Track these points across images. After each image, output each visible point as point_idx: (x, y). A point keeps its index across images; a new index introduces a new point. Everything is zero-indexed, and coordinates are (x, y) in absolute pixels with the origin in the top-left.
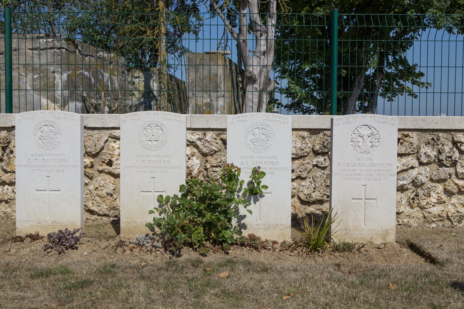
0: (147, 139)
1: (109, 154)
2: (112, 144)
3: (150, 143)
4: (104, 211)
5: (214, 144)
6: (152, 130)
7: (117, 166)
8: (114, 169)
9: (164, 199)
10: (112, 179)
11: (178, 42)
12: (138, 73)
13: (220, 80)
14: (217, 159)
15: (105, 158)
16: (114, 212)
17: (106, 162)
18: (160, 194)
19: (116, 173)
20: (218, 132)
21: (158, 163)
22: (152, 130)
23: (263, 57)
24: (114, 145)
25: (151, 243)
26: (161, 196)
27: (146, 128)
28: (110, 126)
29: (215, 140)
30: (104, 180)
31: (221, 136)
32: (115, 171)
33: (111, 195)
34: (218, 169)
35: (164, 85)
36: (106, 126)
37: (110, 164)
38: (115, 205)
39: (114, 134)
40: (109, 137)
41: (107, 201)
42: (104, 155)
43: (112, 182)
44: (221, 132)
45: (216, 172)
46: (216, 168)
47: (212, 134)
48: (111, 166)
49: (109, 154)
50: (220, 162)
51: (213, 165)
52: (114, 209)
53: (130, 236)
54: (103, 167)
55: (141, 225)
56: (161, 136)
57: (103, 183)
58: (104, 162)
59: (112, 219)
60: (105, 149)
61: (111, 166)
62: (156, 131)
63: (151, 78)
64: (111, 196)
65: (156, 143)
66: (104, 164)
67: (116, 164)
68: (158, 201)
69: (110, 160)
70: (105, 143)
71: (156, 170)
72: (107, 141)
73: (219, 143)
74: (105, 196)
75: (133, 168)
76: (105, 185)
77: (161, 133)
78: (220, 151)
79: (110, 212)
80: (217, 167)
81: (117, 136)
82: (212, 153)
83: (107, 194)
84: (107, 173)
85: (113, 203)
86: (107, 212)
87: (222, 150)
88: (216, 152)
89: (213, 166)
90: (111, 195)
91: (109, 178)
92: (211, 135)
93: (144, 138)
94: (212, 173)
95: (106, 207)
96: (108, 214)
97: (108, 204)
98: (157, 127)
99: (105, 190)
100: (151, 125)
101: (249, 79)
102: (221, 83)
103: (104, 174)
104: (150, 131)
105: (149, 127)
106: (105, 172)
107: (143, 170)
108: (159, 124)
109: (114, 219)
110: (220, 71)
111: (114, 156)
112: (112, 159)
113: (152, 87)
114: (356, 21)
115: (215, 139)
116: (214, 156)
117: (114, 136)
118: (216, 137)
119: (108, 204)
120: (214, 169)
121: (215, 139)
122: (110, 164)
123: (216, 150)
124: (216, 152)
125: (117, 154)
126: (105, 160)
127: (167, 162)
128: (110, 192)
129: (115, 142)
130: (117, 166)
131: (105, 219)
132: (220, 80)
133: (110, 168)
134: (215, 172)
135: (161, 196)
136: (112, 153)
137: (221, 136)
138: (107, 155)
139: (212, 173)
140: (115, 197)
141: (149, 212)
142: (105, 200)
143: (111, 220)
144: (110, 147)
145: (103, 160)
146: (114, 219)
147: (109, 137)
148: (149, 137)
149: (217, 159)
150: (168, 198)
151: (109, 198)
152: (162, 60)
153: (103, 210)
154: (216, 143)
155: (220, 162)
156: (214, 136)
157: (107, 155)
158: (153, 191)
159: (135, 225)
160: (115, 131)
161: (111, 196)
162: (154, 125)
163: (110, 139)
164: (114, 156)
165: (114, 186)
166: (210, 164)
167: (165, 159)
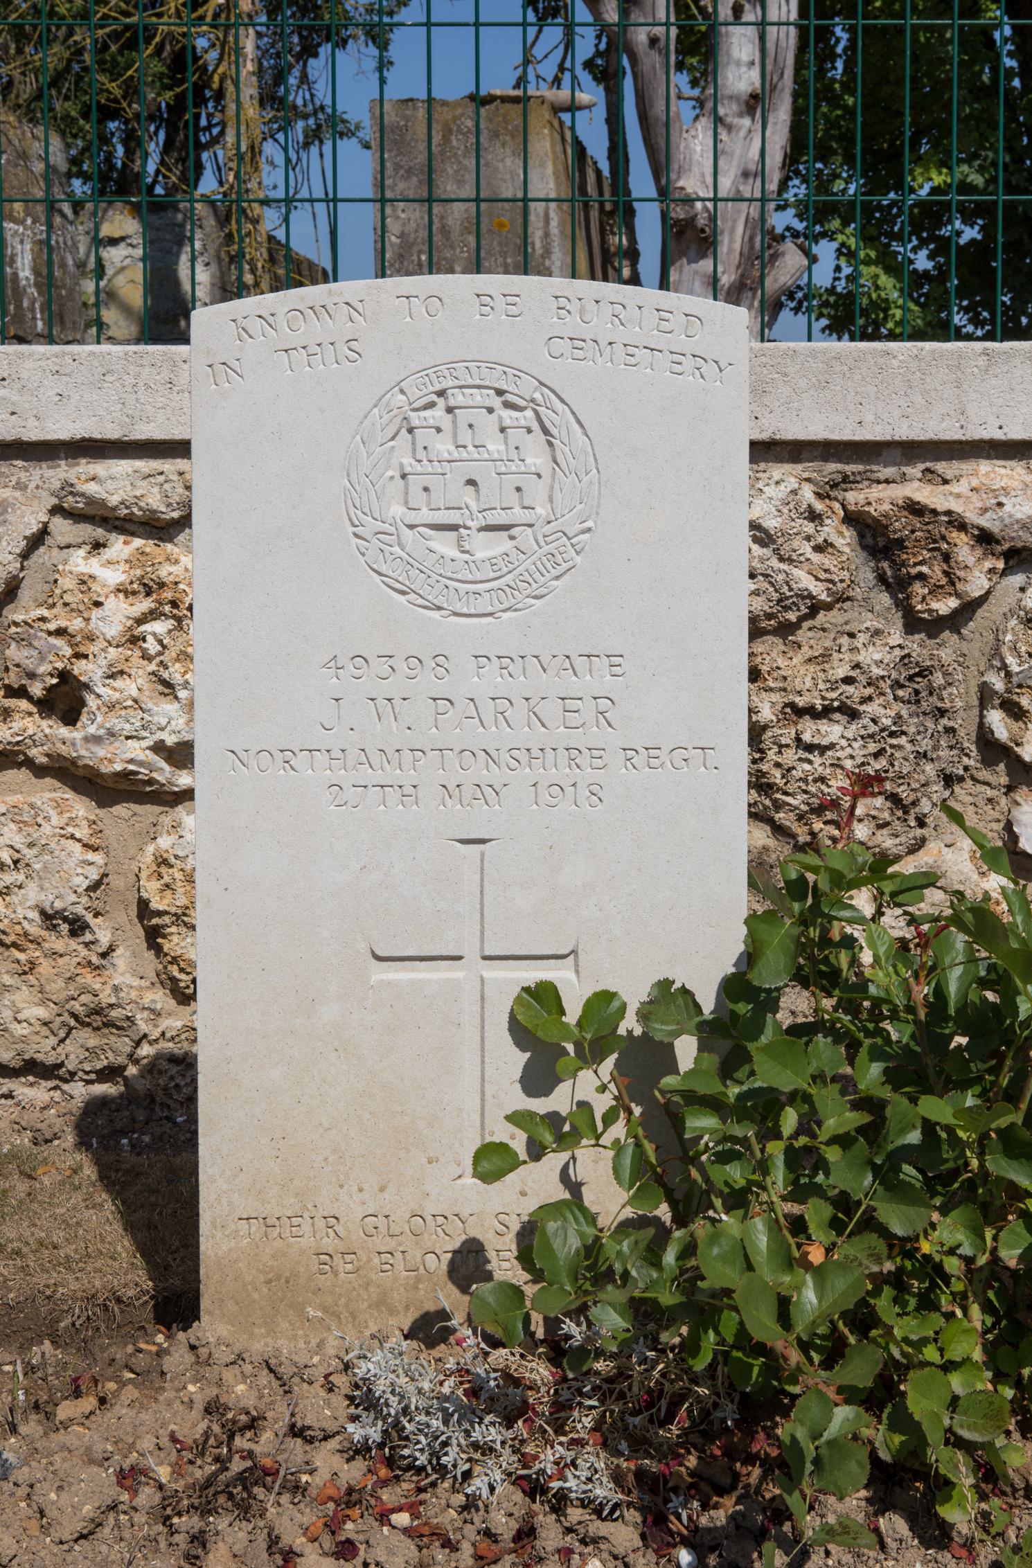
0: (425, 516)
1: (61, 632)
2: (79, 561)
3: (444, 545)
4: (23, 1039)
5: (807, 549)
6: (466, 436)
7: (114, 722)
8: (97, 739)
9: (572, 1016)
10: (82, 807)
11: (293, 81)
12: (121, 222)
13: (547, 235)
14: (825, 656)
15: (29, 664)
16: (93, 1042)
17: (37, 690)
18: (532, 974)
19: (106, 769)
20: (832, 466)
21: (518, 714)
22: (466, 436)
23: (746, 122)
24: (94, 566)
25: (508, 1458)
26: (544, 996)
27: (415, 419)
28: (64, 435)
29: (809, 528)
30: (26, 819)
31: (854, 497)
32: (101, 752)
33: (78, 927)
34: (832, 731)
35: (253, 271)
36: (33, 433)
37: (61, 706)
38: (106, 997)
39: (92, 488)
40: (56, 510)
41: (45, 967)
42: (20, 640)
43: (82, 832)
44: (850, 468)
45: (823, 749)
46: (823, 726)
47: (792, 483)
48: (71, 717)
49: (61, 632)
50: (848, 680)
51: (800, 702)
52: (97, 1021)
53: (289, 1345)
54: (17, 725)
55: (381, 1243)
56: (537, 492)
57: (19, 841)
58: (21, 692)
59: (79, 1090)
60: (25, 595)
61: (71, 717)
62: (495, 446)
63: (180, 244)
64: (74, 933)
65: (501, 543)
66: (24, 704)
67: (111, 707)
68: (520, 1033)
69: (64, 676)
70: (25, 555)
71: (495, 775)
72: (38, 540)
73: (839, 542)
74: (34, 930)
75: (301, 760)
76: (29, 853)
77: (536, 458)
78: (842, 598)
79: (69, 1046)
80: (825, 713)
81: (114, 500)
82: (792, 616)
83: (49, 918)
84: (40, 771)
85: (88, 979)
86: (44, 1049)
87: (857, 592)
88: (816, 608)
89: (800, 712)
90: (78, 927)
91: (58, 806)
92: (784, 489)
93: (397, 510)
94: (790, 757)
95: (42, 1012)
96: (50, 1060)
97: (57, 988)
98: (508, 416)
99: (33, 894)
100: (457, 398)
101: (681, 233)
102: (547, 252)
103: (23, 774)
104: (443, 446)
105: (438, 413)
106: (29, 763)
107: (391, 774)
108: (525, 388)
109: (100, 1089)
110: (546, 181)
111: (91, 649)
112: (81, 669)
113: (187, 287)
114: (855, 103)
115: (813, 516)
116: (802, 635)
117: (91, 501)
118: (819, 506)
119: (57, 988)
120: (810, 730)
121: (813, 516)
122: (61, 706)
123: (819, 590)
124: (816, 608)
125: (113, 629)
126: (32, 676)
127: (588, 709)
128: (70, 901)
129: (98, 546)
130: (114, 722)
131: (34, 1092)
132: (547, 235)
133: (64, 731)
134: (810, 748)
135: (544, 996)
136: (76, 624)
137: (854, 497)
138: (42, 641)
139: (790, 757)
140: (104, 938)
141: (479, 1156)
142: (33, 965)
143: (78, 1103)
144: (67, 583)
145: (13, 679)
146: (100, 1089)
147: (56, 510)
148: (438, 499)
149: (825, 656)
150: (603, 1004)
151: (59, 945)
152: (243, 148)
153: (20, 1030)
154: (818, 549)
155: (848, 680)
156: (808, 493)
157: (42, 641)
158: (471, 950)
159: (329, 1243)
160: (100, 468)
161: (74, 933)
162: (478, 397)
163: (60, 525)
164: (91, 649)
165: (98, 858)
166: (776, 697)
167: (574, 685)
